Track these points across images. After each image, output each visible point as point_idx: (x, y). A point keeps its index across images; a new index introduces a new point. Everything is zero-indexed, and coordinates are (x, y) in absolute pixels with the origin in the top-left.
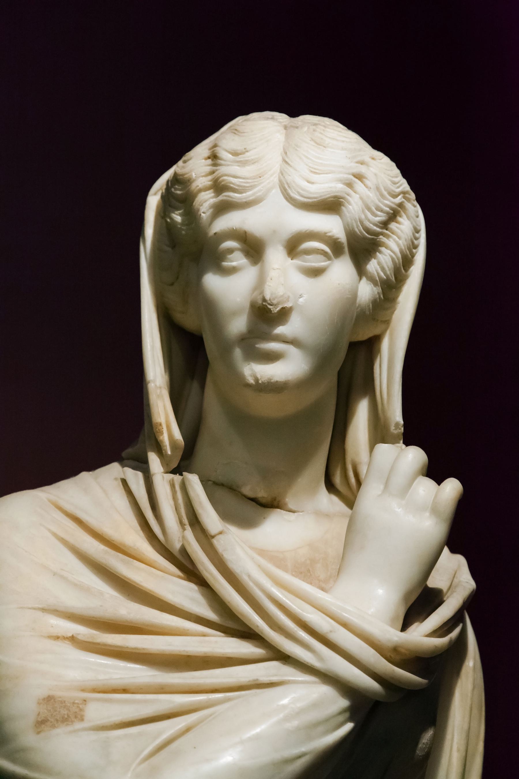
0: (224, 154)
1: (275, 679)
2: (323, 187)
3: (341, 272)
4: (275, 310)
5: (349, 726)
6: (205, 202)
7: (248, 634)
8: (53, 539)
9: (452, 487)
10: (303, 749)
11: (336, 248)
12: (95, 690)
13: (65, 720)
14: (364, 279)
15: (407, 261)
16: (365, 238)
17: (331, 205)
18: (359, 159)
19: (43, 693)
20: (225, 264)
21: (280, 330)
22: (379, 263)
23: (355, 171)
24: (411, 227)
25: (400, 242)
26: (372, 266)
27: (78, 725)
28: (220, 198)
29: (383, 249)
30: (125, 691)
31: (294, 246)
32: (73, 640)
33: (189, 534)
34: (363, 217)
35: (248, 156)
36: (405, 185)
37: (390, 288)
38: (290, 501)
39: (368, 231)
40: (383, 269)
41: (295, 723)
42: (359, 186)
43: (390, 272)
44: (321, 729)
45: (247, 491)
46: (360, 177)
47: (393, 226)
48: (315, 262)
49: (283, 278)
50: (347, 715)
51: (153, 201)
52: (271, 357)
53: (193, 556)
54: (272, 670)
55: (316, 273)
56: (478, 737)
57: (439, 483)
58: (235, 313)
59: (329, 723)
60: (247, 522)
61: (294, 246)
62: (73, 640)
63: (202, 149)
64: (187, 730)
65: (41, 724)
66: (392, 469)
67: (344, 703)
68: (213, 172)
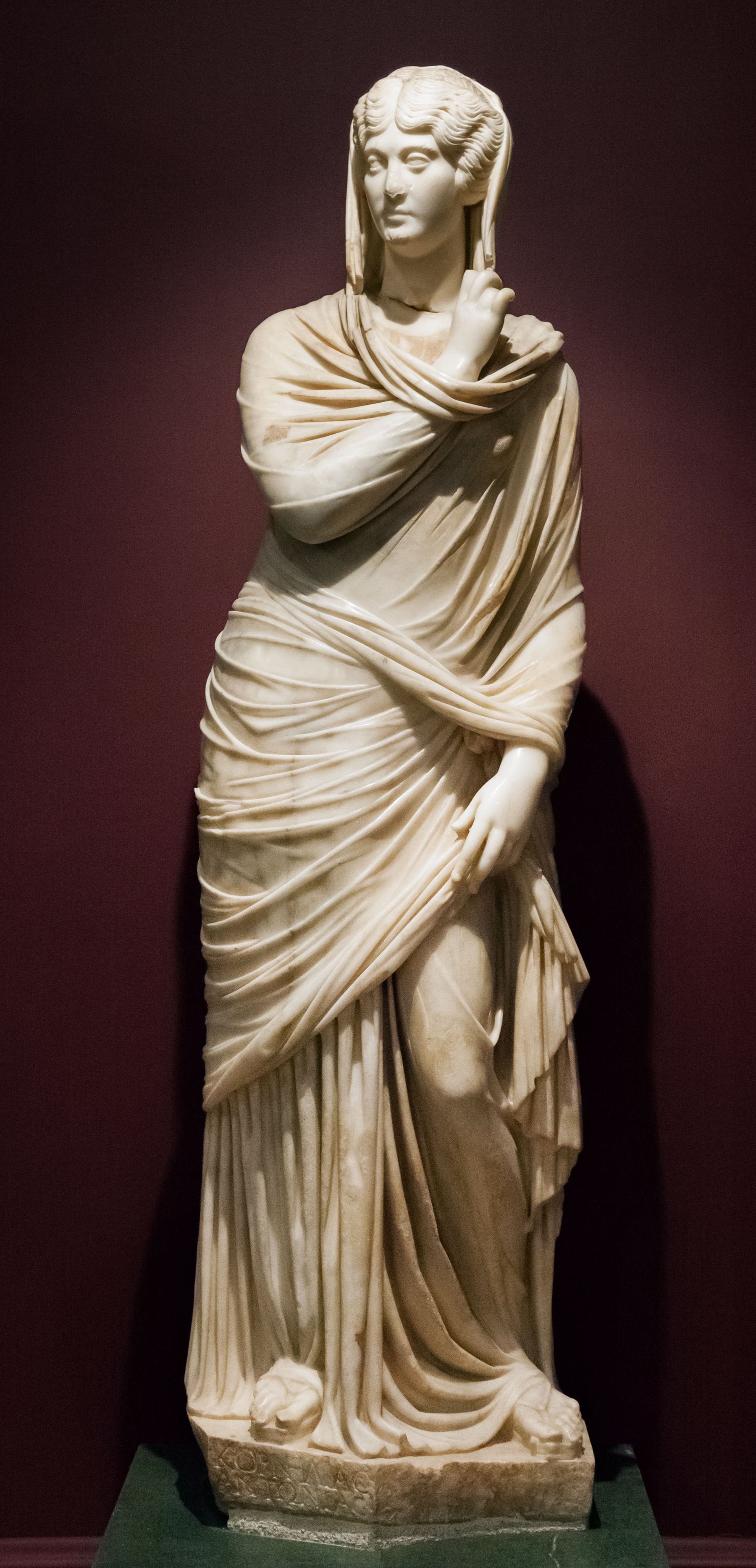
0: (370, 103)
1: (387, 411)
3: (439, 169)
7: (379, 387)
8: (292, 338)
10: (397, 448)
11: (432, 155)
12: (296, 421)
13: (278, 438)
14: (458, 170)
15: (491, 154)
16: (451, 146)
17: (425, 129)
18: (446, 97)
19: (269, 424)
20: (371, 169)
21: (400, 207)
22: (467, 159)
23: (441, 106)
25: (481, 144)
26: (462, 161)
27: (283, 440)
30: (311, 421)
31: (404, 156)
32: (290, 394)
34: (447, 133)
35: (378, 103)
37: (480, 173)
38: (433, 307)
39: (453, 141)
40: (470, 162)
41: (394, 434)
42: (443, 114)
44: (410, 437)
45: (407, 302)
46: (445, 109)
47: (475, 134)
49: (394, 177)
50: (429, 429)
52: (397, 224)
54: (390, 405)
55: (418, 171)
56: (569, 440)
58: (377, 199)
59: (414, 434)
60: (406, 320)
61: (404, 156)
62: (290, 394)
64: (339, 440)
65: (267, 440)
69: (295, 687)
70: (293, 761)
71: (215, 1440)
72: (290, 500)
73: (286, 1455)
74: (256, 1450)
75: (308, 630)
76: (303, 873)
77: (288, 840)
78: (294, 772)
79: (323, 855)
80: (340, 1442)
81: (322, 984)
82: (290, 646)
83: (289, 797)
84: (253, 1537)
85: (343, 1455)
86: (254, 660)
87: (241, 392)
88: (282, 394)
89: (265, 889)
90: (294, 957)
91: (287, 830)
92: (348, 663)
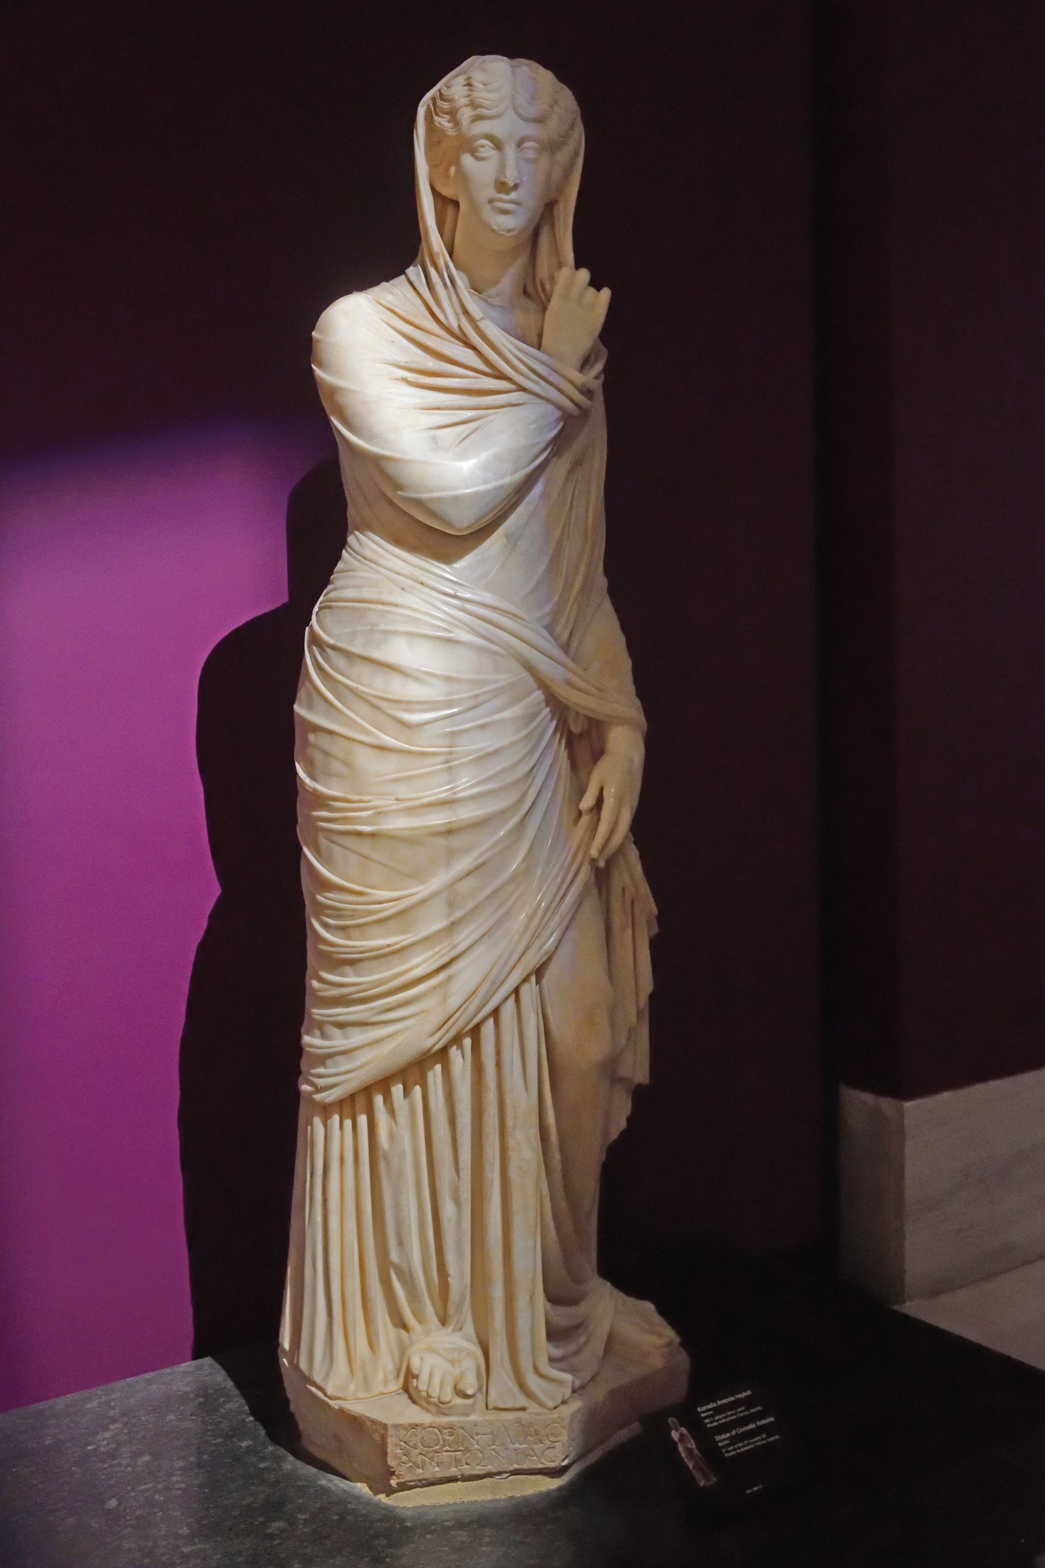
0: (478, 85)
5: (561, 424)
6: (466, 114)
9: (606, 293)
30: (439, 409)
32: (405, 380)
33: (464, 321)
51: (421, 111)
54: (516, 397)
62: (405, 380)
67: (558, 414)
68: (469, 96)
70: (451, 753)
72: (431, 491)
80: (522, 1401)
83: (448, 790)
84: (746, 1391)
85: (528, 1411)
87: (320, 365)
89: (422, 883)
90: (455, 946)
91: (450, 823)
92: (495, 653)
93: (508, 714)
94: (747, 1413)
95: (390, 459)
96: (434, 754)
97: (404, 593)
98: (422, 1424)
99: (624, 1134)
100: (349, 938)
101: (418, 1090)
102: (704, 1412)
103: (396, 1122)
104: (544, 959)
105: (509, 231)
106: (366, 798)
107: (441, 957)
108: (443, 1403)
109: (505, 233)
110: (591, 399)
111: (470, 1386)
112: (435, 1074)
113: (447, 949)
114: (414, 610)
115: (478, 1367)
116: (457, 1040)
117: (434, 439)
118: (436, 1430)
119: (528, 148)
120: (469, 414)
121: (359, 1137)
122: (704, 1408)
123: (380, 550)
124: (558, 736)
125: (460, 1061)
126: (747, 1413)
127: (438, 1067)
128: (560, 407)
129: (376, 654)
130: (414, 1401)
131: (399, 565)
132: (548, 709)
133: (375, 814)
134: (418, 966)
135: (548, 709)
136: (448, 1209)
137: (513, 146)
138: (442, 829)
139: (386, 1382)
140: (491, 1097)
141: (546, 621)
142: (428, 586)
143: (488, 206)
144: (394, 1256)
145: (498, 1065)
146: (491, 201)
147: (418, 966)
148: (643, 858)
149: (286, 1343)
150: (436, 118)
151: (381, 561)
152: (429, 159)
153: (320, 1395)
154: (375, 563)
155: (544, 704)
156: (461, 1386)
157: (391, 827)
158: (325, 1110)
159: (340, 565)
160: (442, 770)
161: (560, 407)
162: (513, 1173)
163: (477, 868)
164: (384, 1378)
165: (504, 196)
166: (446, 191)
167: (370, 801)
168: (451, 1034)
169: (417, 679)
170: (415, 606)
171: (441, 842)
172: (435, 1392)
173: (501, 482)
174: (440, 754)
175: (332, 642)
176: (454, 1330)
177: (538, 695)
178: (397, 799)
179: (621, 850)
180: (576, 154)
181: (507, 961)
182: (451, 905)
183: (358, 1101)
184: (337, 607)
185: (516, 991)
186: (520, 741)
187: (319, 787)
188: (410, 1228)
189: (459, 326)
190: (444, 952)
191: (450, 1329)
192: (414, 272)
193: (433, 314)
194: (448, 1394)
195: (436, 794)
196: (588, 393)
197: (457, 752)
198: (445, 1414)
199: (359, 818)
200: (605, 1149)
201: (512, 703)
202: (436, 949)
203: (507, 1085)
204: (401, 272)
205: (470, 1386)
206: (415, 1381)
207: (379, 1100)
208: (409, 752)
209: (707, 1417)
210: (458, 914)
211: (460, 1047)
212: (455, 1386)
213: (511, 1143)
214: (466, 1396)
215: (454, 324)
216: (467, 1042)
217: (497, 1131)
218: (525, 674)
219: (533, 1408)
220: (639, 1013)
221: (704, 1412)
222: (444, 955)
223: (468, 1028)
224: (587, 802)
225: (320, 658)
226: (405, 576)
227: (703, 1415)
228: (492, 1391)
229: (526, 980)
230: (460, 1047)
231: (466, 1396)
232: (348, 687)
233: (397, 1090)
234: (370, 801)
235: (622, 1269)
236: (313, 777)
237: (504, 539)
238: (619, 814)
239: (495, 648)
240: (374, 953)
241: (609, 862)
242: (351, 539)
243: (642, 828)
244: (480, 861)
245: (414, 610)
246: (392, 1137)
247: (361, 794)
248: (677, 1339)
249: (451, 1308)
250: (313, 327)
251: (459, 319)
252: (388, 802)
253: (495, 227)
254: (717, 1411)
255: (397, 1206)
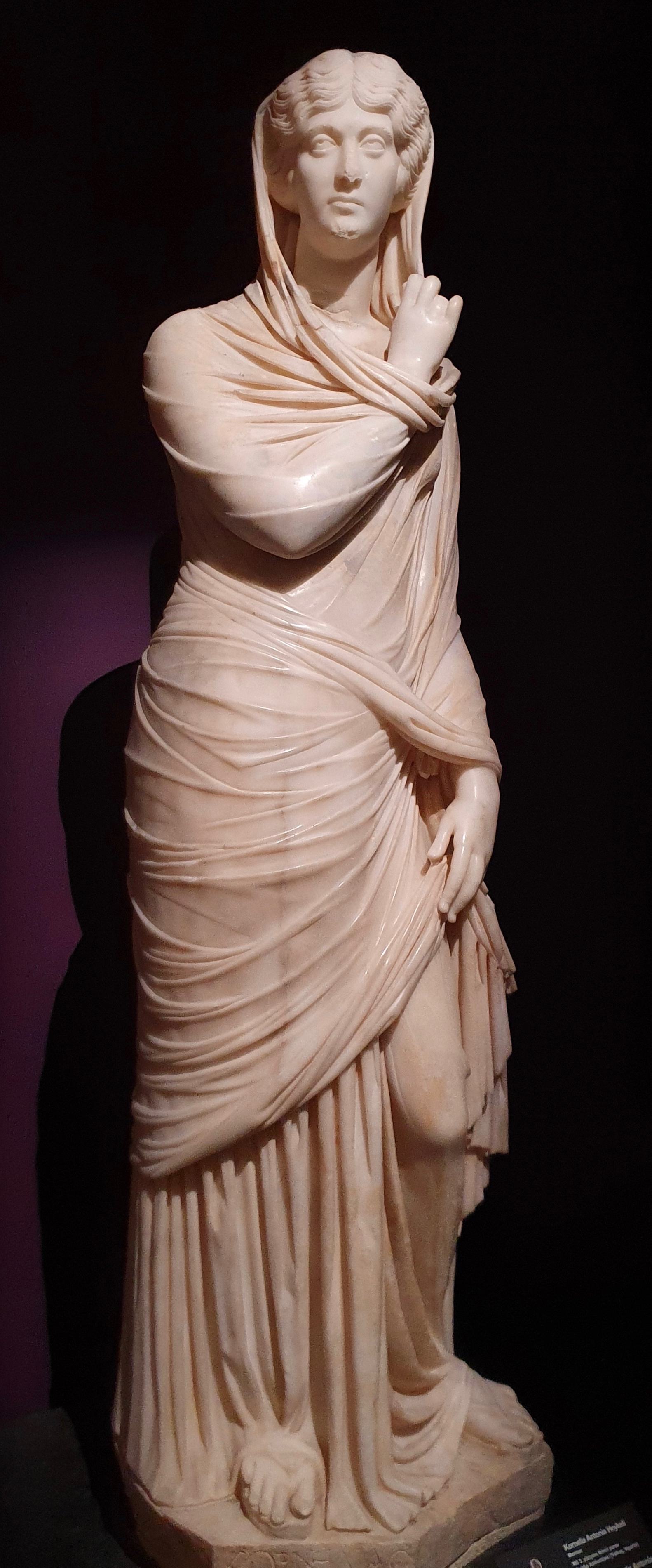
1: (361, 414)
2: (382, 96)
4: (352, 180)
5: (408, 440)
7: (342, 388)
9: (457, 301)
17: (384, 110)
24: (425, 137)
26: (405, 154)
28: (314, 105)
29: (412, 144)
32: (237, 393)
33: (301, 329)
36: (425, 104)
37: (417, 170)
42: (401, 97)
43: (416, 162)
46: (401, 91)
48: (375, 148)
51: (259, 118)
52: (346, 212)
53: (305, 343)
57: (449, 299)
61: (363, 134)
62: (237, 393)
63: (298, 75)
66: (421, 290)
67: (405, 427)
68: (305, 89)
69: (282, 716)
70: (283, 797)
71: (224, 1549)
72: (267, 509)
73: (311, 1549)
74: (272, 1552)
75: (288, 654)
76: (298, 918)
77: (282, 883)
78: (280, 810)
79: (320, 898)
80: (364, 1521)
81: (206, 1012)
82: (270, 672)
84: (618, 1522)
85: (372, 1534)
86: (227, 687)
88: (226, 392)
90: (288, 1010)
91: (283, 873)
92: (333, 688)
93: (349, 754)
94: (621, 1552)
95: (216, 476)
96: (265, 798)
97: (234, 624)
98: (252, 1548)
99: (480, 1208)
100: (174, 998)
101: (251, 1166)
102: (572, 1550)
103: (226, 1202)
104: (388, 1024)
105: (351, 233)
106: (190, 846)
107: (273, 1022)
108: (276, 1525)
109: (346, 236)
110: (443, 417)
111: (306, 1500)
112: (269, 1151)
113: (281, 1012)
114: (244, 642)
115: (317, 1475)
116: (292, 1114)
117: (266, 453)
118: (267, 1554)
119: (371, 141)
120: (306, 427)
121: (189, 1212)
122: (572, 1546)
123: (211, 580)
124: (405, 778)
125: (296, 1137)
126: (621, 1552)
127: (272, 1143)
128: (405, 420)
129: (203, 691)
130: (246, 1514)
131: (236, 597)
132: (393, 750)
133: (200, 864)
134: (249, 1030)
135: (393, 750)
136: (284, 1300)
137: (354, 138)
138: (275, 879)
139: (217, 1487)
140: (331, 1178)
141: (391, 655)
142: (260, 617)
143: (328, 207)
144: (226, 1346)
145: (339, 1141)
146: (330, 202)
147: (249, 1030)
148: (498, 910)
149: (117, 1429)
150: (273, 119)
151: (212, 591)
152: (268, 167)
153: (146, 1497)
154: (205, 593)
155: (388, 744)
156: (296, 1504)
157: (218, 877)
158: (154, 1185)
159: (173, 598)
160: (275, 815)
161: (405, 420)
162: (355, 1265)
163: (313, 923)
164: (215, 1486)
165: (344, 195)
166: (286, 201)
167: (194, 849)
168: (284, 1108)
169: (248, 717)
170: (245, 638)
171: (270, 893)
172: (266, 1509)
173: (339, 499)
174: (272, 797)
175: (158, 678)
176: (291, 1431)
177: (381, 735)
178: (224, 848)
179: (472, 902)
180: (425, 157)
181: (345, 1028)
182: (285, 963)
183: (187, 1177)
184: (167, 641)
185: (357, 1061)
186: (361, 783)
187: (144, 834)
188: (242, 1317)
189: (297, 338)
190: (277, 1015)
191: (287, 1429)
192: (253, 290)
193: (270, 328)
194: (280, 1513)
195: (265, 842)
196: (442, 411)
197: (288, 796)
198: (276, 1536)
199: (183, 867)
200: (456, 1241)
201: (354, 741)
202: (268, 1013)
203: (348, 1165)
204: (241, 291)
205: (306, 1500)
206: (246, 1489)
207: (208, 1178)
208: (239, 796)
209: (575, 1558)
210: (292, 973)
211: (296, 1120)
212: (290, 1500)
213: (352, 1231)
214: (299, 1516)
215: (292, 336)
216: (304, 1117)
217: (337, 1215)
218: (367, 712)
219: (378, 1530)
220: (497, 1078)
221: (572, 1550)
222: (275, 1020)
223: (304, 1101)
224: (438, 848)
225: (147, 696)
226: (235, 606)
227: (570, 1555)
228: (332, 1507)
229: (368, 1047)
230: (296, 1120)
231: (299, 1516)
232: (174, 726)
233: (228, 1167)
234: (194, 849)
235: (480, 1348)
236: (139, 824)
237: (344, 565)
238: (471, 864)
239: (332, 682)
240: (200, 1016)
241: (462, 915)
242: (184, 571)
243: (496, 877)
244: (315, 916)
245: (244, 642)
246: (222, 1216)
247: (186, 842)
248: (539, 1435)
249: (289, 1409)
250: (144, 348)
251: (297, 329)
252: (215, 851)
253: (335, 230)
254: (589, 1548)
255: (228, 1293)
